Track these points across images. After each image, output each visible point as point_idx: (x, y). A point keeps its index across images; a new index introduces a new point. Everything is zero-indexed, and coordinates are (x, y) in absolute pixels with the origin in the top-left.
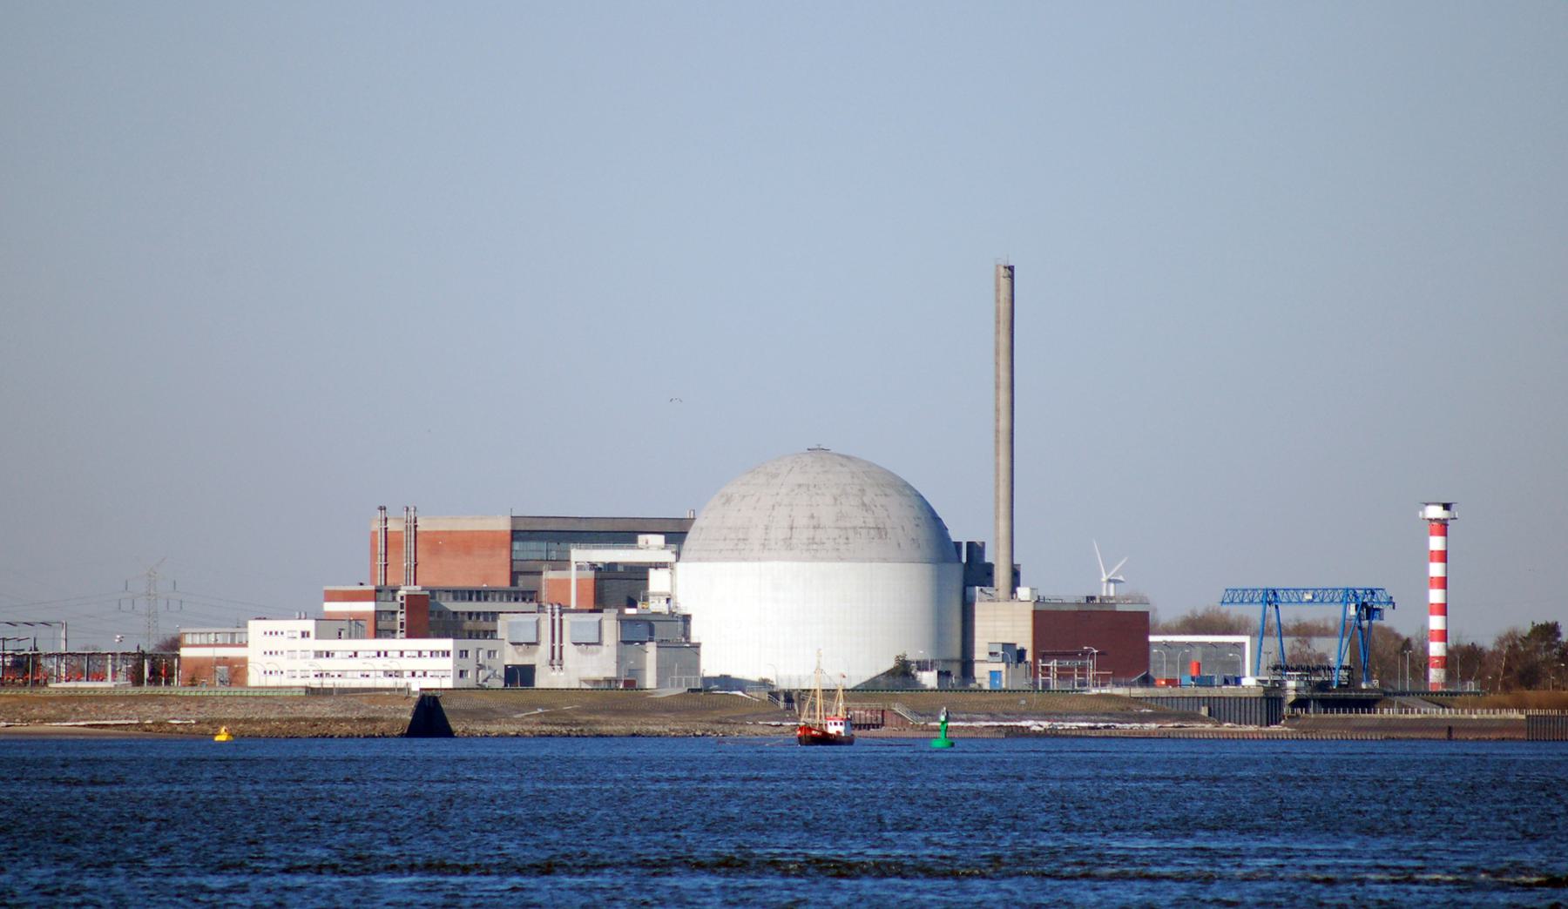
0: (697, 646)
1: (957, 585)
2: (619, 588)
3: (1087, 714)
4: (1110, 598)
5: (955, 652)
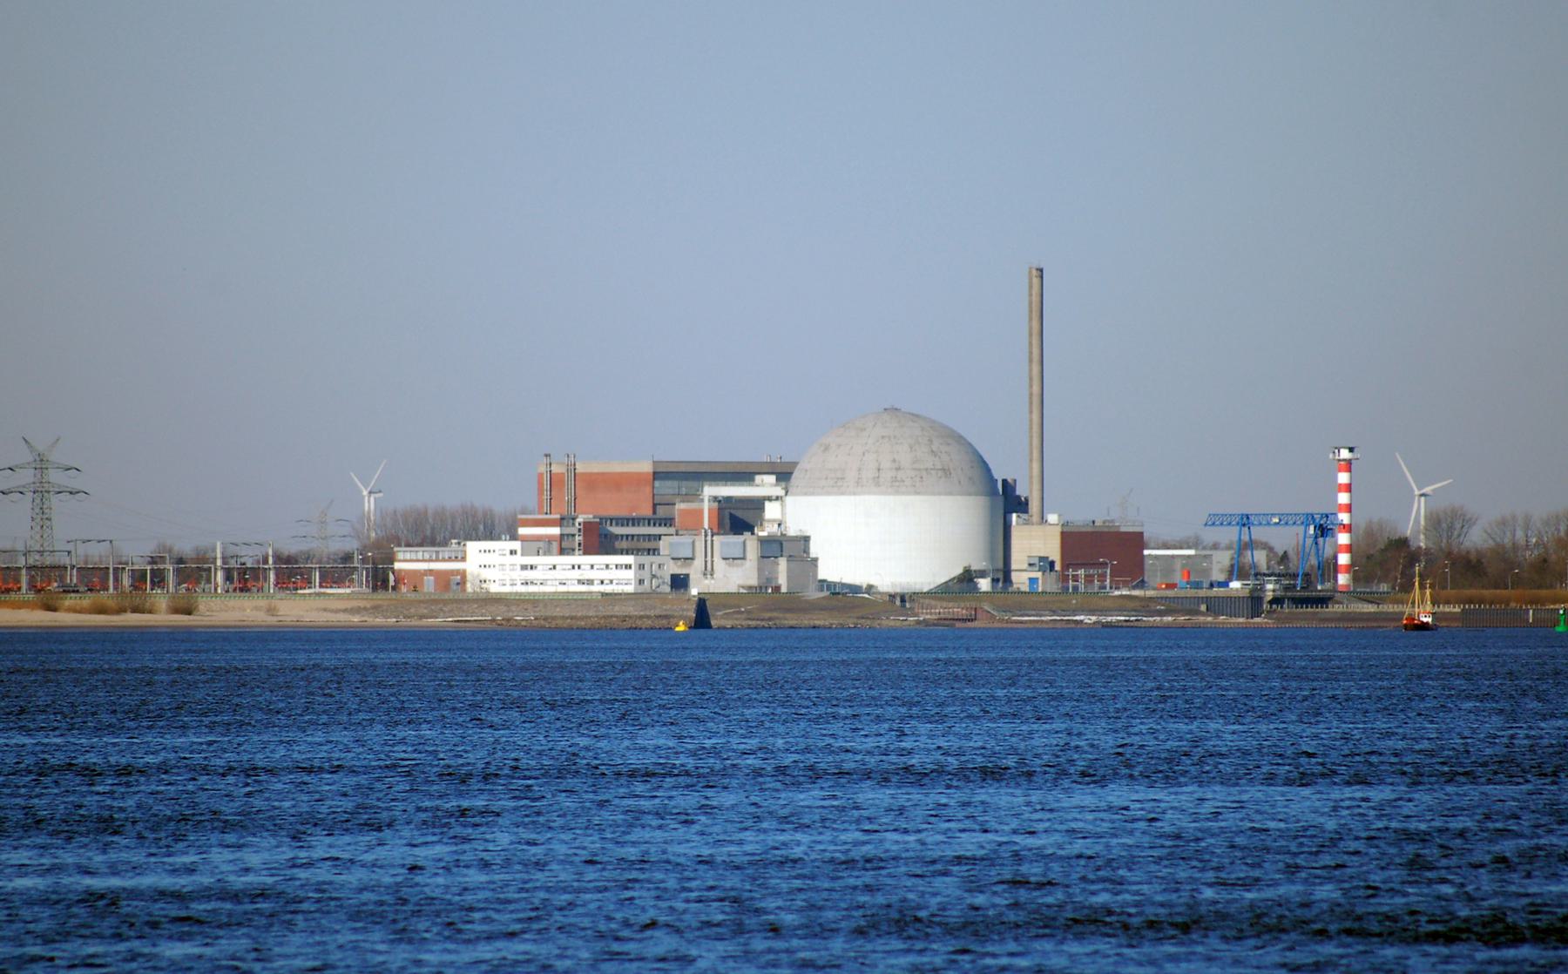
0: (816, 560)
1: (1001, 512)
2: (738, 519)
3: (1120, 610)
4: (1515, 547)
5: (1000, 565)
